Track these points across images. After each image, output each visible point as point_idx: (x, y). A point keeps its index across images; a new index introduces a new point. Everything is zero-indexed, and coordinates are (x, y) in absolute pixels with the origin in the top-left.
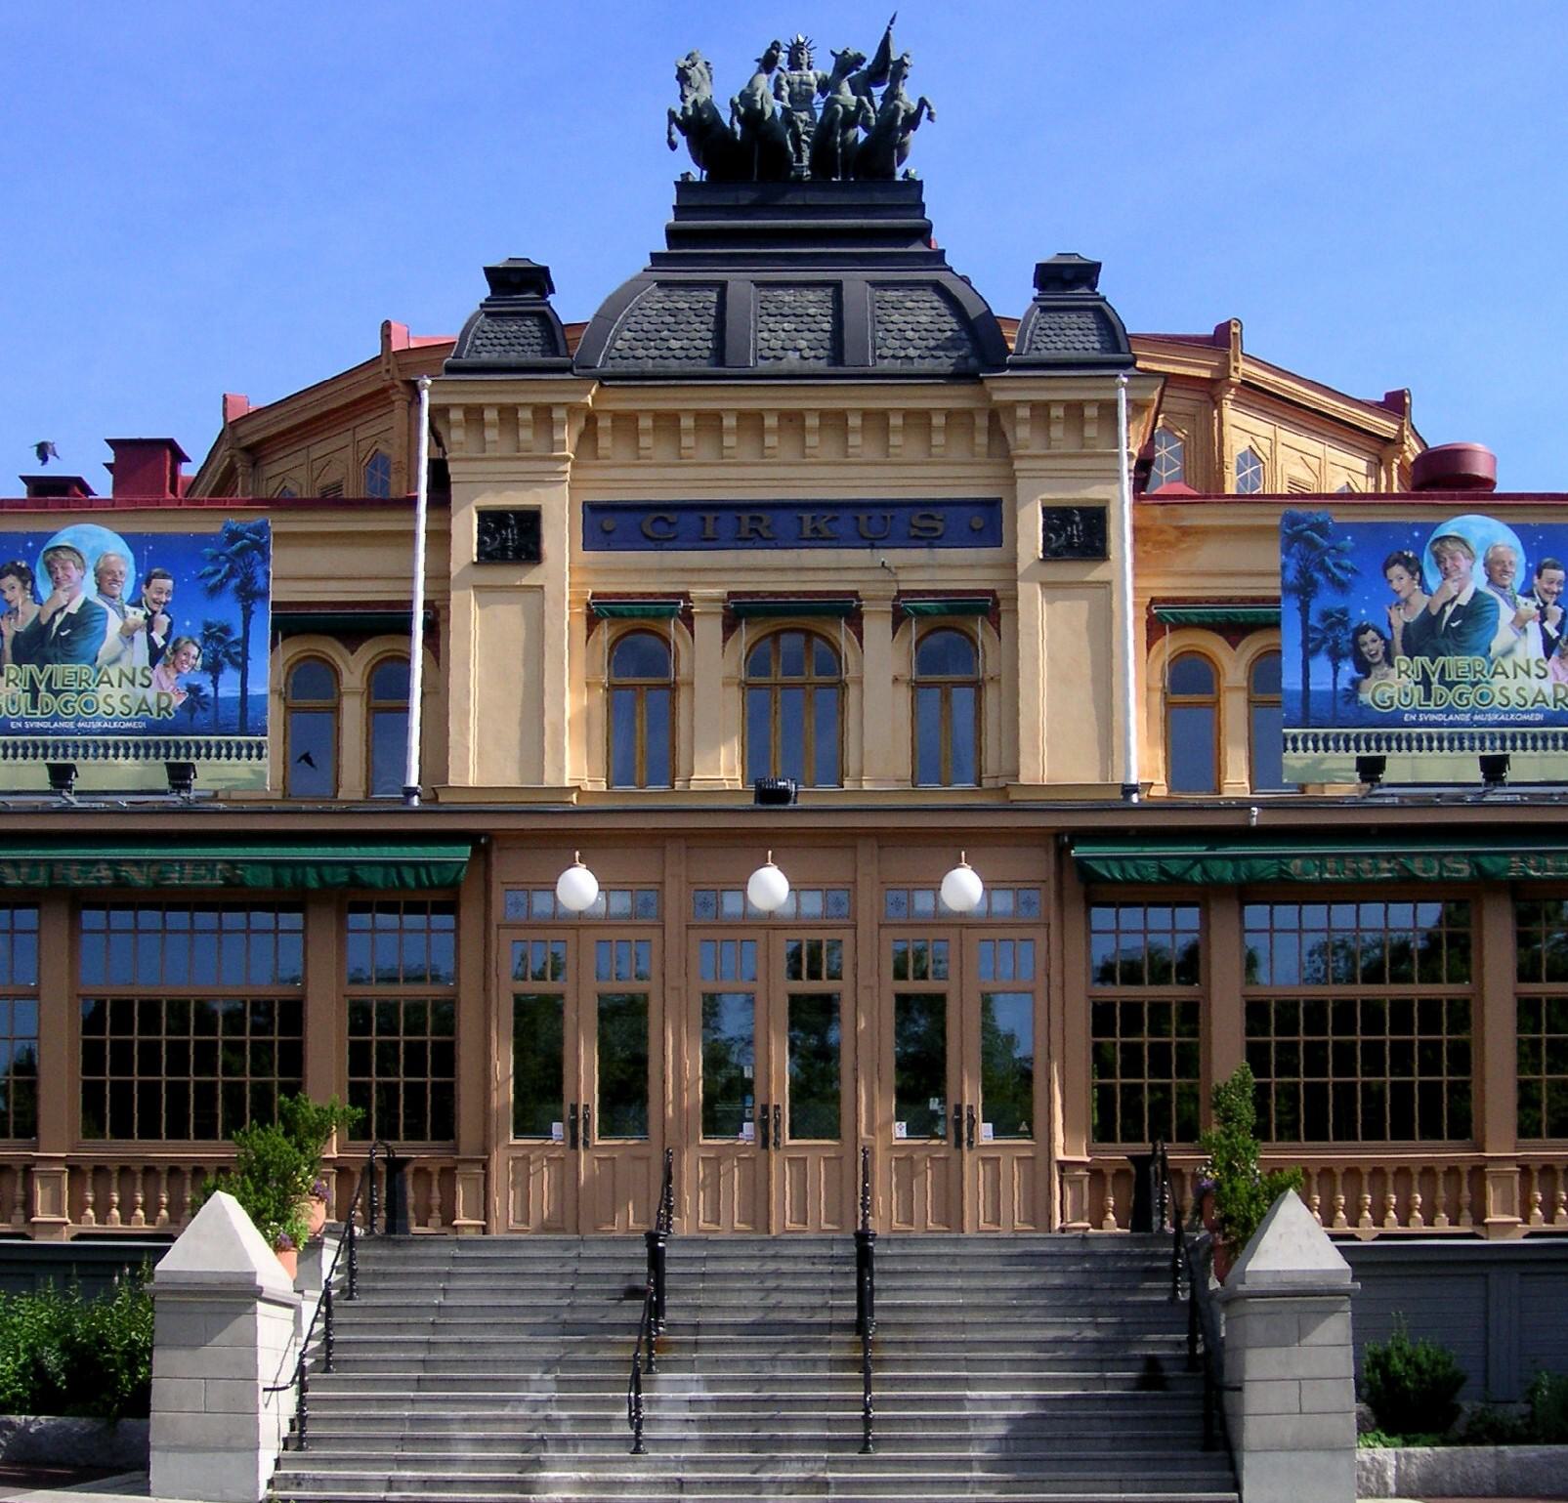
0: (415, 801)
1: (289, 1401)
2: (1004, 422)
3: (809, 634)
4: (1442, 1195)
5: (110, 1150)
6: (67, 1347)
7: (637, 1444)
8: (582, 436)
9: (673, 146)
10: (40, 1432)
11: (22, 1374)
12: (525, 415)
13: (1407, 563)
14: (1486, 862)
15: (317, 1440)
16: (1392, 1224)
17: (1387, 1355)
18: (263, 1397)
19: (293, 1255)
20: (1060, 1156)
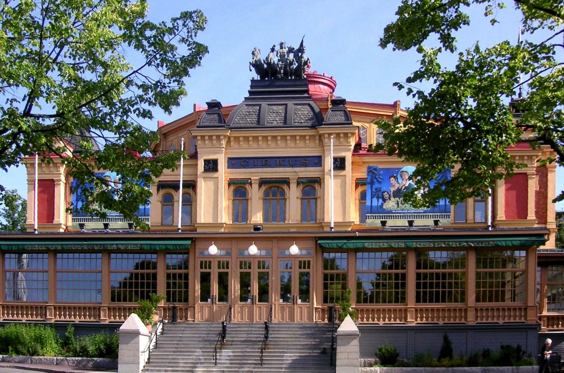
0: (180, 231)
1: (146, 355)
2: (322, 138)
3: (278, 187)
4: (398, 315)
5: (116, 304)
6: (105, 344)
7: (216, 364)
8: (227, 142)
9: (251, 70)
10: (100, 361)
11: (96, 350)
12: (214, 137)
13: (394, 177)
14: (408, 244)
15: (151, 362)
16: (387, 321)
17: (382, 348)
18: (140, 354)
19: (150, 326)
20: (315, 306)
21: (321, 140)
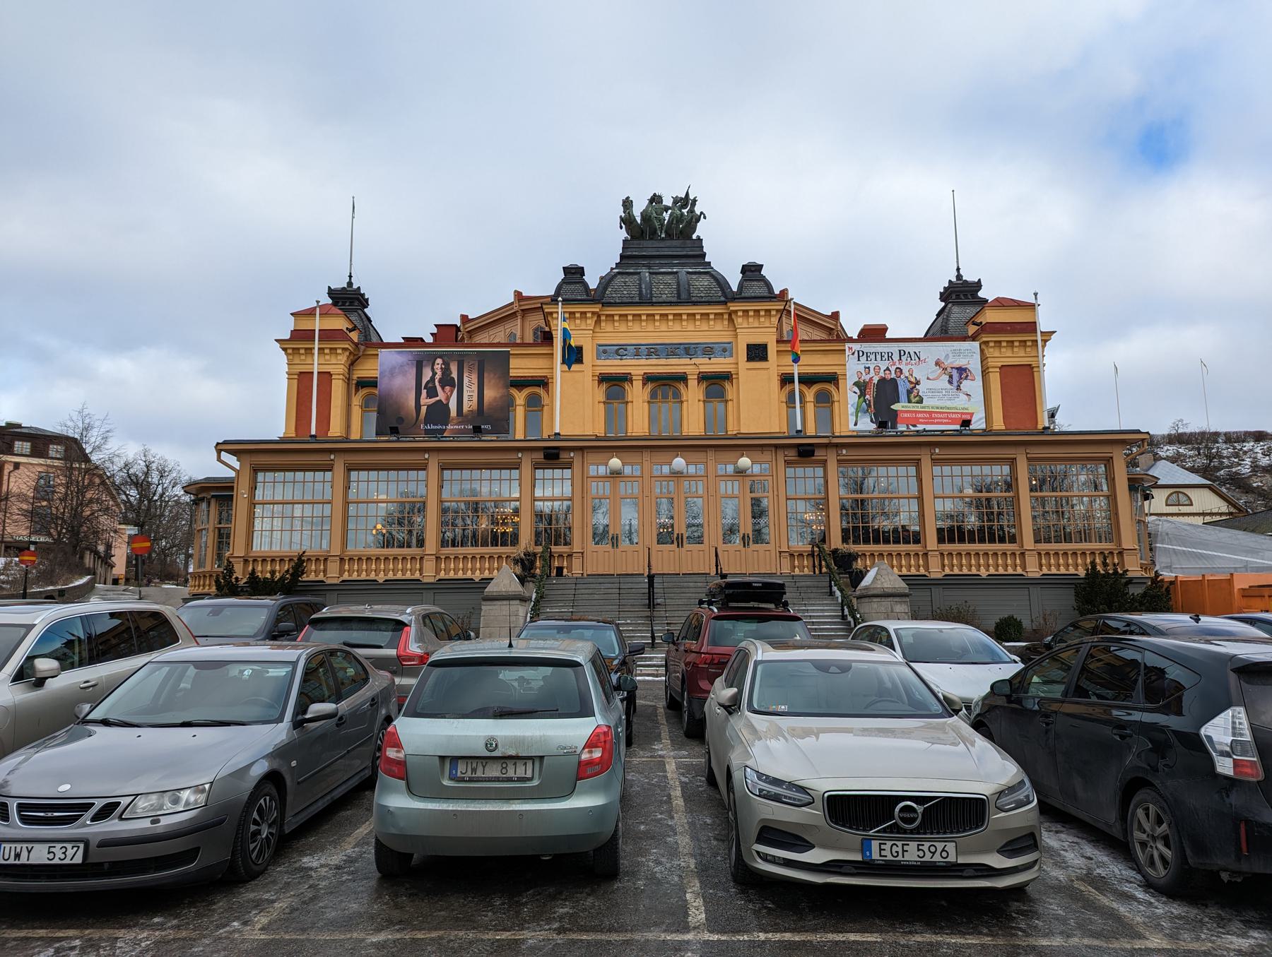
21: (731, 320)
